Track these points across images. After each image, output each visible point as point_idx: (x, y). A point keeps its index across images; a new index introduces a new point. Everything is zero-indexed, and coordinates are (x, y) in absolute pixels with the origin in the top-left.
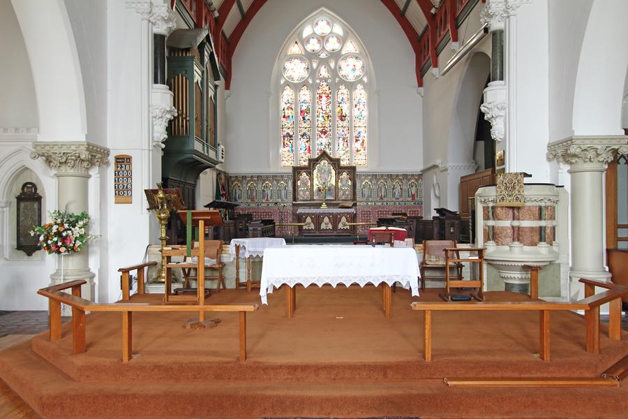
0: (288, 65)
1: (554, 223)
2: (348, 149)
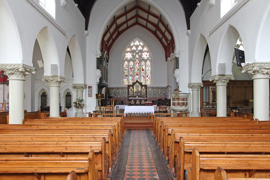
0: (126, 54)
1: (187, 102)
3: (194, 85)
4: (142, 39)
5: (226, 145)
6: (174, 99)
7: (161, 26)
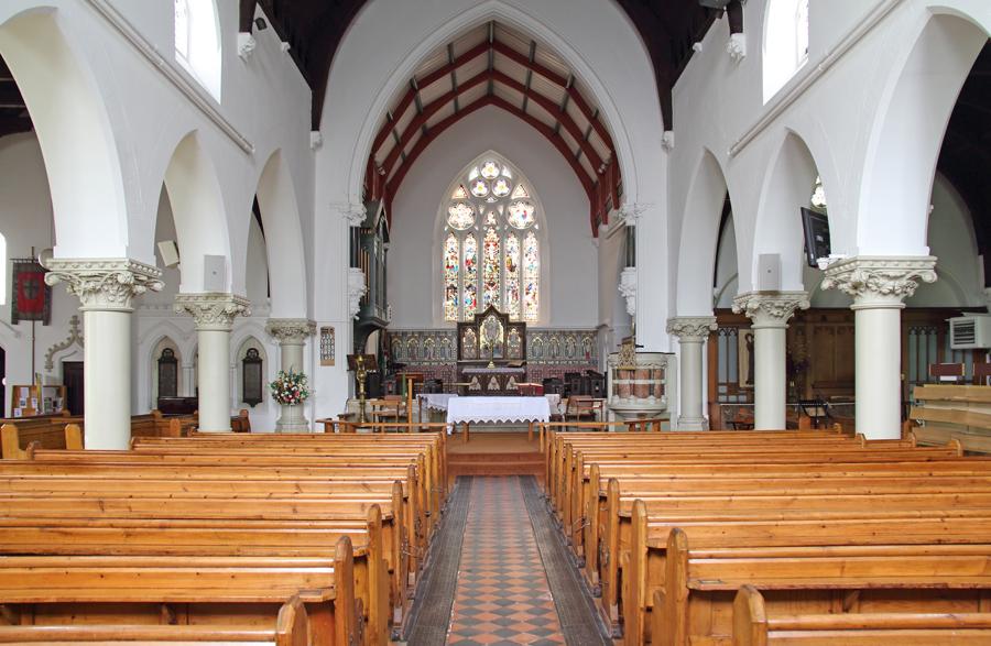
0: (452, 211)
1: (663, 382)
3: (687, 322)
4: (507, 156)
5: (733, 498)
7: (574, 110)
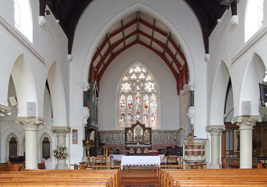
0: (123, 85)
1: (204, 150)
2: (148, 120)
3: (214, 127)
4: (145, 64)
6: (187, 147)
7: (170, 46)
